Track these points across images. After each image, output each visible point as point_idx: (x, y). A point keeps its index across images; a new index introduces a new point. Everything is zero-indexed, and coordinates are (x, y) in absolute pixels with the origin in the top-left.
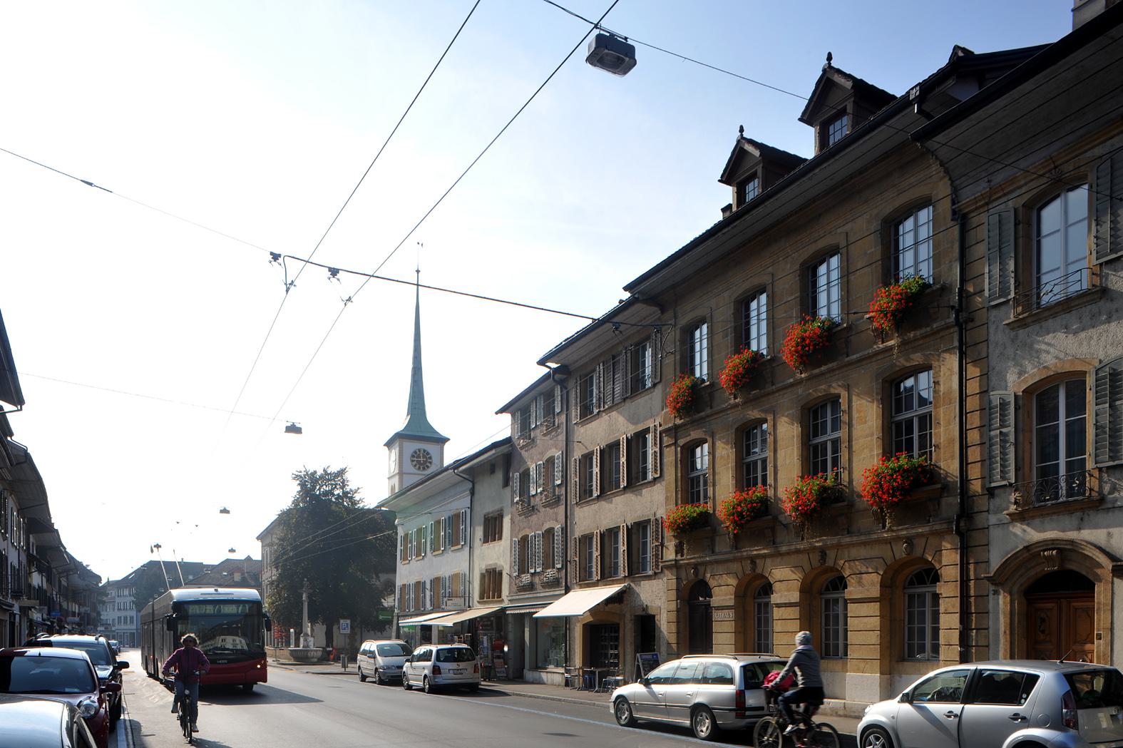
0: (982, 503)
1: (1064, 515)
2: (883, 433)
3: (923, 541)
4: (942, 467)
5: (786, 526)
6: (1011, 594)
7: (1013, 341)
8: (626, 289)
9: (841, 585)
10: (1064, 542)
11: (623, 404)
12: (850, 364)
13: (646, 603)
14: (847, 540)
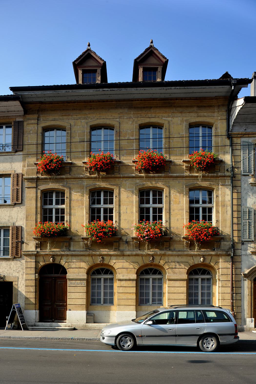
0: (239, 246)
2: (41, 204)
3: (210, 257)
4: (220, 230)
5: (127, 242)
6: (251, 281)
7: (251, 190)
8: (12, 89)
9: (200, 273)
11: (13, 154)
12: (171, 177)
13: (4, 274)
14: (170, 253)
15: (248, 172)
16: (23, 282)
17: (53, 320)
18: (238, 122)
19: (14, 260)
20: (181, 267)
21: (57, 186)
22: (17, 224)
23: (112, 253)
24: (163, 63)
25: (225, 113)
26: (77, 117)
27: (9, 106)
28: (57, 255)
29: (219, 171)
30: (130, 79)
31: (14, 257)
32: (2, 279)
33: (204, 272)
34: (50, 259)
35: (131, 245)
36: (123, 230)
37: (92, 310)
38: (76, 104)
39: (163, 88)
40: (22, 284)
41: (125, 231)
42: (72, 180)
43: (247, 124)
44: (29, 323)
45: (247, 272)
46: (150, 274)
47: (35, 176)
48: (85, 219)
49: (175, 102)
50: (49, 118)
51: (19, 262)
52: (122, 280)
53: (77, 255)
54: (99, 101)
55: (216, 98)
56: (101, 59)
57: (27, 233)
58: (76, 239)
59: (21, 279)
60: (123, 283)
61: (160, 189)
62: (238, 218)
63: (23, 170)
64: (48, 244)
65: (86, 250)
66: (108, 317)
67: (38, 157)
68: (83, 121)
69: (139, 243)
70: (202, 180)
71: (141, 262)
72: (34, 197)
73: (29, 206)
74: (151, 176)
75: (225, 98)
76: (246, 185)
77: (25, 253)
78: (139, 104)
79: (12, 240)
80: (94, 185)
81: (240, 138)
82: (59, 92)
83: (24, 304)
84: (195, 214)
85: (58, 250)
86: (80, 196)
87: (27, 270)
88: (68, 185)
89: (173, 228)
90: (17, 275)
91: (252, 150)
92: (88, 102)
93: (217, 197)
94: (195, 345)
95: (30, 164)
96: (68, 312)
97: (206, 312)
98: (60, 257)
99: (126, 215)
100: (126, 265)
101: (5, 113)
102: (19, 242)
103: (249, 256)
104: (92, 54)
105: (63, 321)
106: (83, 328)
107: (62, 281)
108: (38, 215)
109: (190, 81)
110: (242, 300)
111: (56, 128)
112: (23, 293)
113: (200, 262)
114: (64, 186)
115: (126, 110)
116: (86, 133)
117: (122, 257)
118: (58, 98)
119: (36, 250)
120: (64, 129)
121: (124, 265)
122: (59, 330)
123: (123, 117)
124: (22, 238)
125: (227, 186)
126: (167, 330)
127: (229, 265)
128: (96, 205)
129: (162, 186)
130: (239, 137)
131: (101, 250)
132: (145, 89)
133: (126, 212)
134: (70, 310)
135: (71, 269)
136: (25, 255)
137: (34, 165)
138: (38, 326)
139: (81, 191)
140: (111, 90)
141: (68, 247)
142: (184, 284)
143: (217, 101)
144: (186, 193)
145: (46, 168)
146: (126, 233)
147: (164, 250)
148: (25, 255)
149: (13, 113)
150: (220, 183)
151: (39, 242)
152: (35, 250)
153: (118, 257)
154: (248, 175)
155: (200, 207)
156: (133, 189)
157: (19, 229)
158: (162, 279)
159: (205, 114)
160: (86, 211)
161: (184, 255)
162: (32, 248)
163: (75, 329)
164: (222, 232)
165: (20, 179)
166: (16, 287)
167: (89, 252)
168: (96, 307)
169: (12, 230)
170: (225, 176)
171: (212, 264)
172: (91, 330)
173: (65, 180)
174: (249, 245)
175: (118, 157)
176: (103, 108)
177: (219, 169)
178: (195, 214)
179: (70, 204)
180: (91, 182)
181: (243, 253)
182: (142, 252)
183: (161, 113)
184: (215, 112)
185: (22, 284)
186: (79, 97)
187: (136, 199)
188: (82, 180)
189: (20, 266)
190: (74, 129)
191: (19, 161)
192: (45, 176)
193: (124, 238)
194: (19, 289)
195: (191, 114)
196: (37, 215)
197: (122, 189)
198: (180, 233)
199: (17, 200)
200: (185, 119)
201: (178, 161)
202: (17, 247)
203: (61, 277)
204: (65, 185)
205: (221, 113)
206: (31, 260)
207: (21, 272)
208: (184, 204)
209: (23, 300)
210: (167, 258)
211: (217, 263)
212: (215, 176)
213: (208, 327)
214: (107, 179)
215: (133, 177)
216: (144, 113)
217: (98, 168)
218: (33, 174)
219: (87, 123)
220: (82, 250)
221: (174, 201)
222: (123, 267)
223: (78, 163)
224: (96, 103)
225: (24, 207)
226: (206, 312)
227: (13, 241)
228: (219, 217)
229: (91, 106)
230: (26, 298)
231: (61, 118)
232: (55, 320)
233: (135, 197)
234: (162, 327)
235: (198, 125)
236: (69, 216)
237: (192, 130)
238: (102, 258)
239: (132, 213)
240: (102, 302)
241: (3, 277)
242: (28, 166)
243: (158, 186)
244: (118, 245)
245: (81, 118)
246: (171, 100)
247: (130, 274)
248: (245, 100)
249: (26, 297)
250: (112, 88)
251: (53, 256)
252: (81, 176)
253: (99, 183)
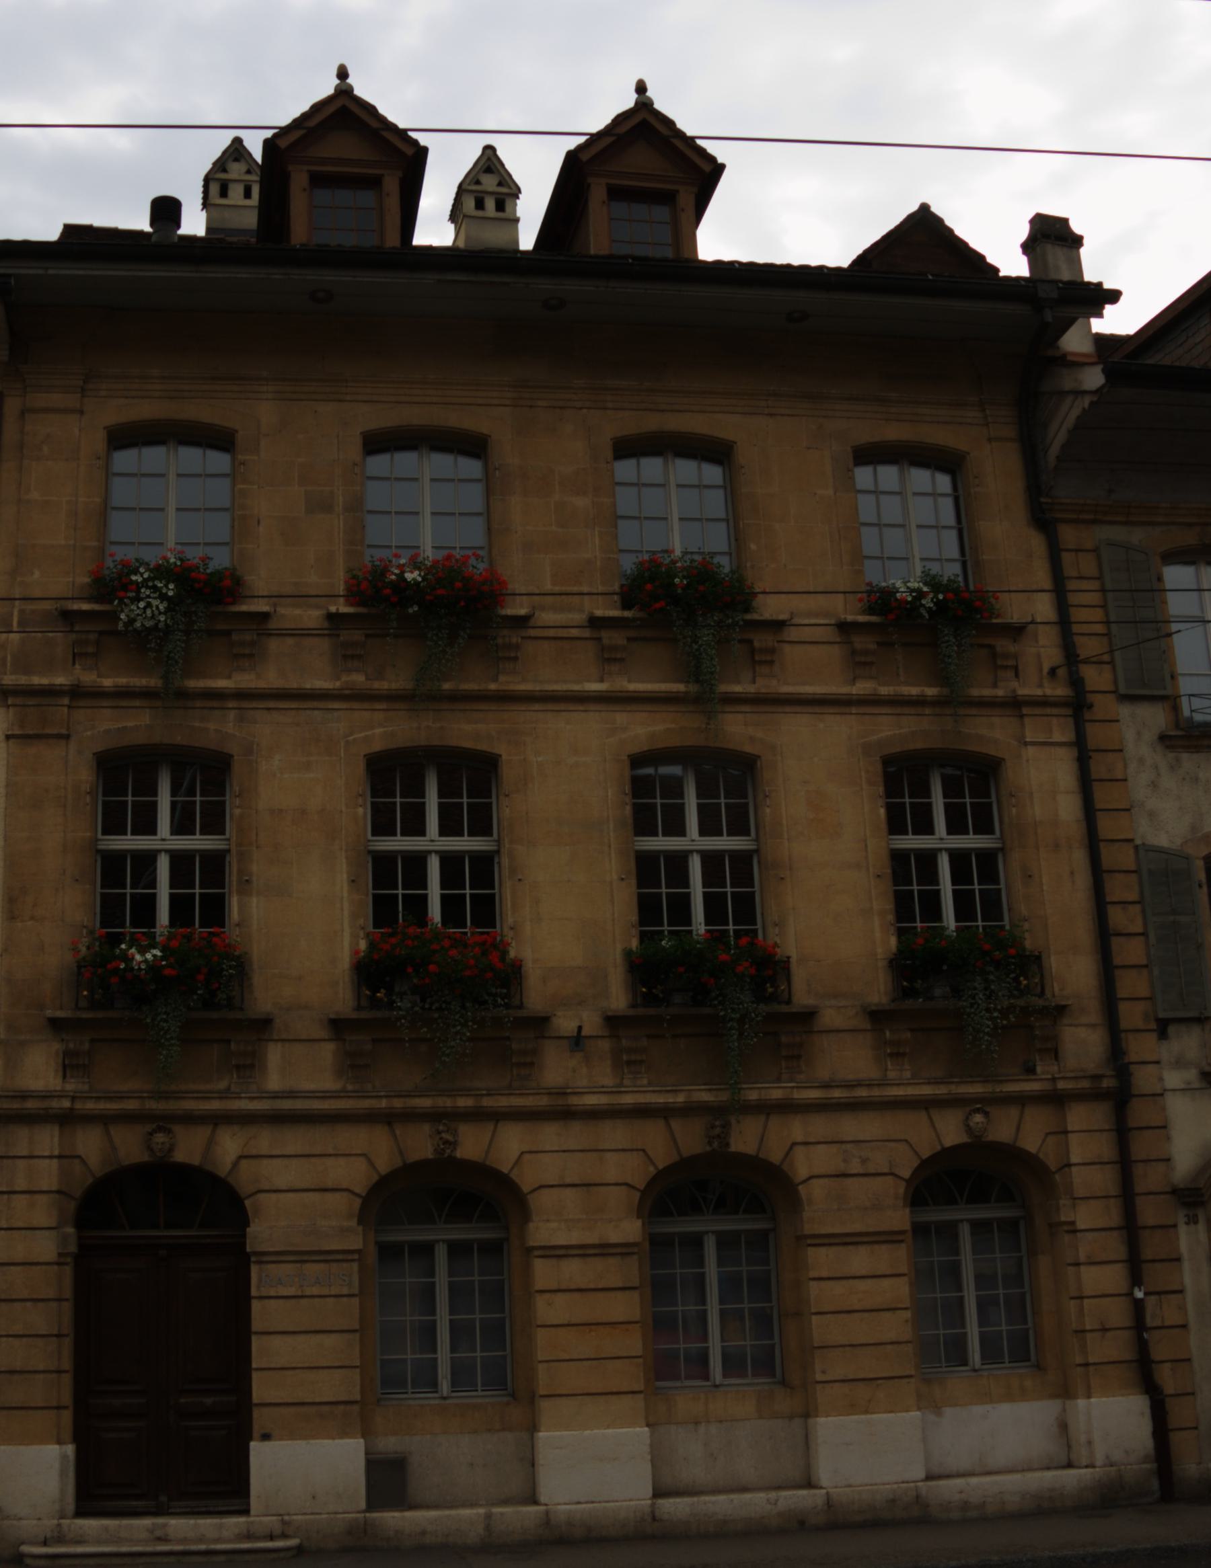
44: (24, 1522)
48: (346, 913)
60: (573, 1271)
71: (660, 1145)
96: (256, 1448)
134: (266, 1437)
138: (79, 1542)
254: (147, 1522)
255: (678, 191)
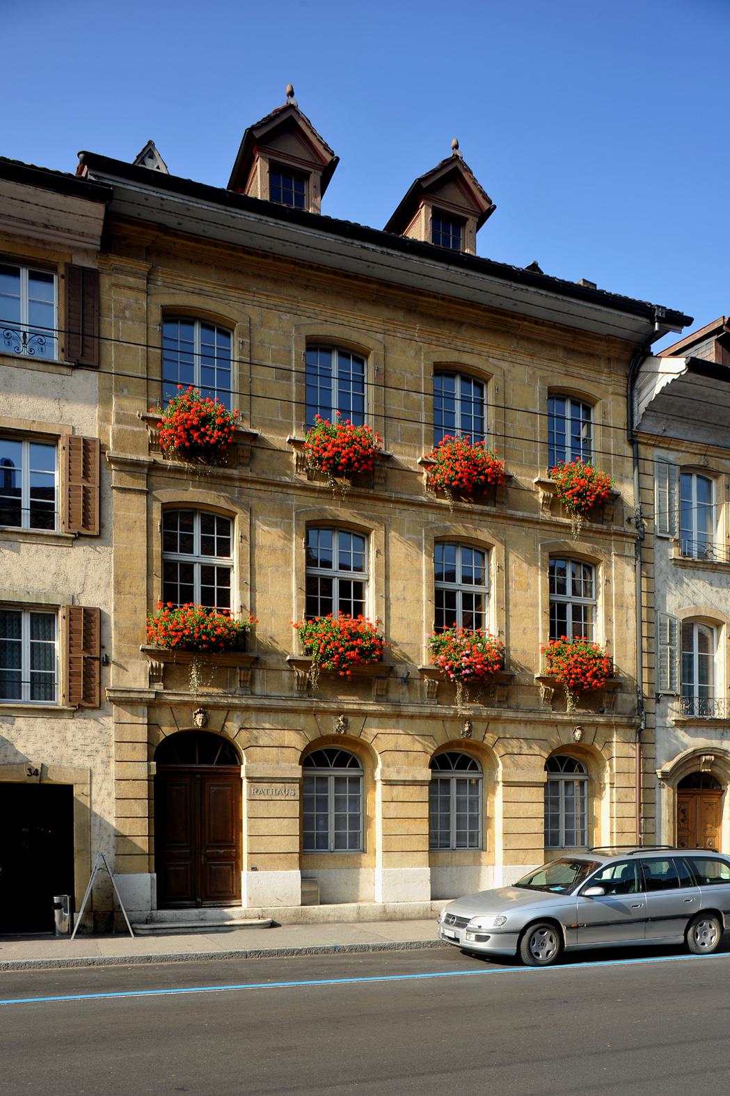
0: (651, 705)
1: (135, 494)
5: (407, 681)
9: (453, 766)
10: (719, 751)
12: (512, 518)
13: (40, 761)
14: (510, 714)
15: (668, 533)
16: (110, 786)
17: (199, 900)
18: (655, 410)
19: (76, 715)
20: (532, 752)
21: (213, 496)
22: (84, 602)
23: (371, 707)
24: (480, 212)
25: (622, 381)
26: (270, 302)
27: (61, 211)
28: (217, 707)
29: (612, 520)
30: (220, 179)
31: (77, 704)
32: (37, 774)
33: (344, 759)
34: (195, 717)
35: (416, 690)
36: (396, 648)
37: (312, 868)
38: (270, 261)
39: (509, 283)
40: (104, 792)
41: (400, 651)
42: (258, 487)
43: (670, 417)
45: (667, 767)
46: (329, 766)
47: (144, 458)
48: (294, 605)
49: (519, 325)
50: (185, 284)
51: (92, 721)
52: (394, 783)
53: (274, 709)
54: (335, 271)
55: (609, 339)
56: (326, 147)
57: (119, 633)
58: (271, 661)
59: (102, 776)
61: (481, 545)
62: (648, 637)
63: (102, 431)
64: (194, 672)
65: (301, 695)
66: (352, 884)
67: (153, 400)
68: (286, 317)
69: (442, 683)
70: (583, 538)
72: (141, 522)
73: (126, 548)
74: (465, 507)
75: (626, 342)
76: (663, 563)
77: (118, 695)
78: (435, 306)
79: (70, 652)
80: (319, 511)
81: (652, 448)
82: (239, 216)
83: (113, 852)
84: (216, 586)
85: (216, 690)
86: (279, 537)
87: (123, 749)
88: (244, 499)
89: (515, 651)
90: (89, 764)
91: (675, 481)
92: (303, 266)
93: (608, 583)
94: (681, 939)
95: (124, 414)
97: (694, 862)
98: (223, 714)
99: (516, 618)
100: (404, 741)
101: (34, 228)
102: (94, 659)
103: (669, 729)
104: (301, 123)
105: (227, 902)
106: (294, 920)
107: (224, 786)
108: (153, 580)
109: (483, 259)
110: (657, 834)
111: (199, 319)
112: (108, 820)
113: (572, 742)
114: (233, 502)
115: (400, 315)
116: (294, 354)
117: (393, 721)
118: (209, 225)
119: (151, 686)
120: (226, 327)
121: (399, 741)
122: (234, 928)
123: (392, 334)
124: (104, 647)
125: (627, 559)
126: (627, 907)
127: (632, 750)
128: (319, 568)
129: (490, 540)
130: (650, 445)
131: (340, 697)
132: (467, 275)
133: (404, 599)
135: (258, 748)
136: (113, 701)
137: (141, 421)
138: (162, 922)
139: (281, 522)
140: (382, 252)
141: (248, 684)
142: (539, 794)
143: (608, 347)
144: (542, 564)
145: (189, 438)
146: (405, 656)
147: (493, 707)
148: (113, 701)
149: (62, 234)
150: (613, 548)
151: (162, 665)
152: (147, 687)
153: (384, 720)
154: (667, 539)
155: (569, 602)
156: (420, 537)
157: (92, 618)
158: (361, 779)
159: (582, 372)
160: (297, 583)
161: (540, 721)
162: (138, 679)
163: (273, 925)
164: (618, 669)
165: (95, 457)
166: (85, 803)
167: (309, 703)
168: (321, 860)
169: (70, 620)
170: (623, 535)
171: (598, 747)
172: (316, 923)
173: (237, 484)
174: (670, 705)
175: (381, 441)
176: (339, 294)
177: (613, 515)
178: (444, 609)
179: (252, 559)
180: (310, 501)
181: (659, 722)
182: (448, 710)
183: (486, 345)
184: (603, 373)
185: (106, 794)
186: (284, 245)
187: (429, 566)
188: (285, 490)
189: (97, 734)
190: (261, 334)
191: (86, 401)
192: (177, 463)
193: (401, 670)
194: (96, 809)
195: (554, 366)
196: (150, 581)
197: (392, 534)
198: (530, 666)
199: (86, 524)
200: (539, 373)
201: (525, 480)
202: (88, 675)
203: (221, 773)
204: (236, 499)
205: (615, 379)
206: (135, 719)
207: (102, 755)
208: (538, 592)
209: (108, 843)
210: (500, 727)
211: (608, 743)
212: (604, 531)
213: (705, 896)
214: (355, 500)
215: (422, 505)
216: (446, 336)
217: (341, 465)
218: (136, 449)
219: (297, 327)
220: (287, 694)
221: (517, 583)
222: (396, 747)
223: (274, 439)
224: (325, 275)
225: (109, 548)
226: (694, 862)
227: (72, 655)
228: (612, 633)
229: (309, 280)
230: (120, 837)
231: (221, 291)
232: (202, 901)
233: (425, 559)
234: (619, 901)
235: (564, 395)
236: (249, 593)
237: (171, 329)
238: (343, 720)
239: (419, 601)
240: (332, 845)
241: (39, 769)
242: (118, 421)
243: (480, 538)
244: (385, 687)
245: (281, 309)
246: (513, 317)
247: (414, 768)
248: (688, 365)
249: (119, 832)
250: (388, 247)
251: (205, 709)
252: (283, 480)
253: (331, 508)
254: (196, 911)
255: (467, 219)
